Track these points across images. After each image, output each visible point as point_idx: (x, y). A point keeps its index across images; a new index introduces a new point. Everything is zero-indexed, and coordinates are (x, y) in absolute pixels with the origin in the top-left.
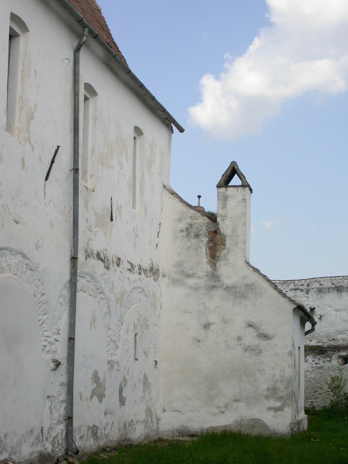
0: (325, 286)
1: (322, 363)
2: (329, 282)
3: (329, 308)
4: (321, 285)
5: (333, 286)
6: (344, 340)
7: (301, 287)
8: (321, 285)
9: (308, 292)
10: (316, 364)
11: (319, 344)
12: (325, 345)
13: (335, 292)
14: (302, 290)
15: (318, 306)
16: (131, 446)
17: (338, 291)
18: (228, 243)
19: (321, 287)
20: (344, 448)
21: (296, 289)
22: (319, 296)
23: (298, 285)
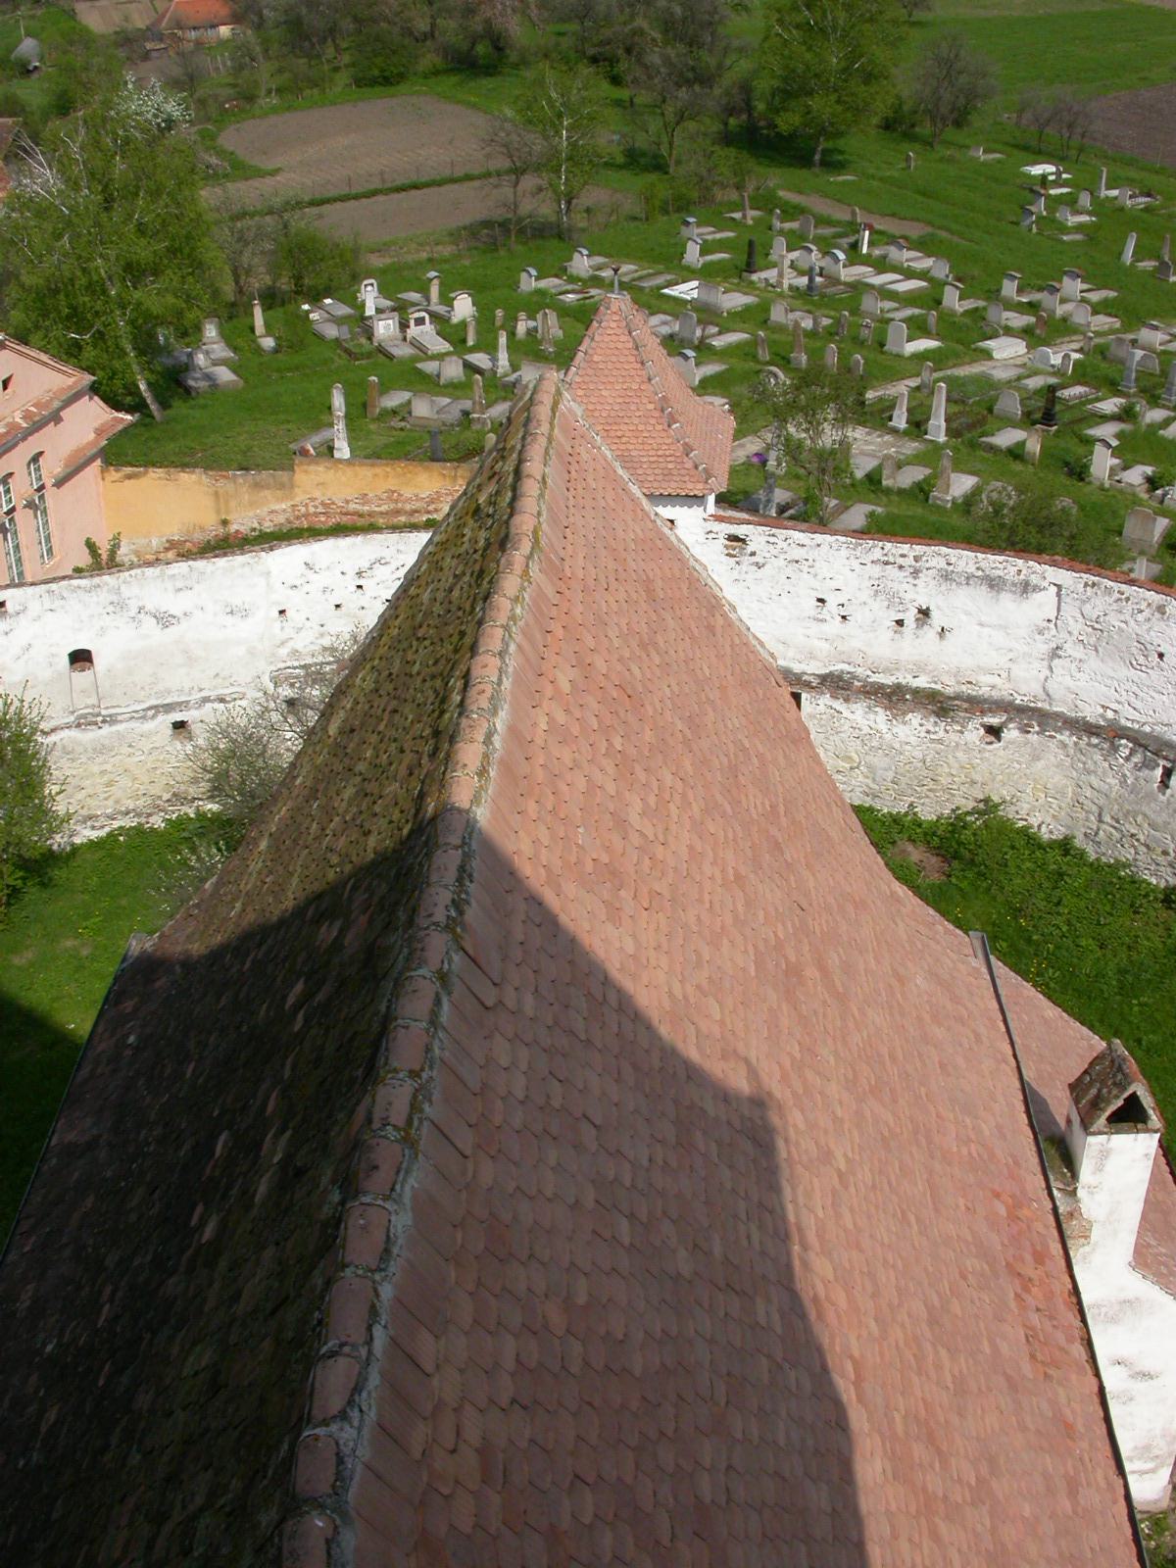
0: (959, 569)
1: (942, 734)
2: (971, 562)
3: (964, 618)
4: (949, 564)
5: (980, 573)
6: (993, 687)
7: (901, 561)
8: (949, 564)
9: (916, 573)
10: (928, 732)
11: (933, 686)
12: (949, 691)
13: (984, 588)
14: (901, 567)
15: (938, 608)
16: (207, 468)
17: (991, 587)
18: (1095, 1235)
19: (951, 568)
20: (777, 207)
21: (887, 563)
22: (943, 588)
23: (894, 555)
